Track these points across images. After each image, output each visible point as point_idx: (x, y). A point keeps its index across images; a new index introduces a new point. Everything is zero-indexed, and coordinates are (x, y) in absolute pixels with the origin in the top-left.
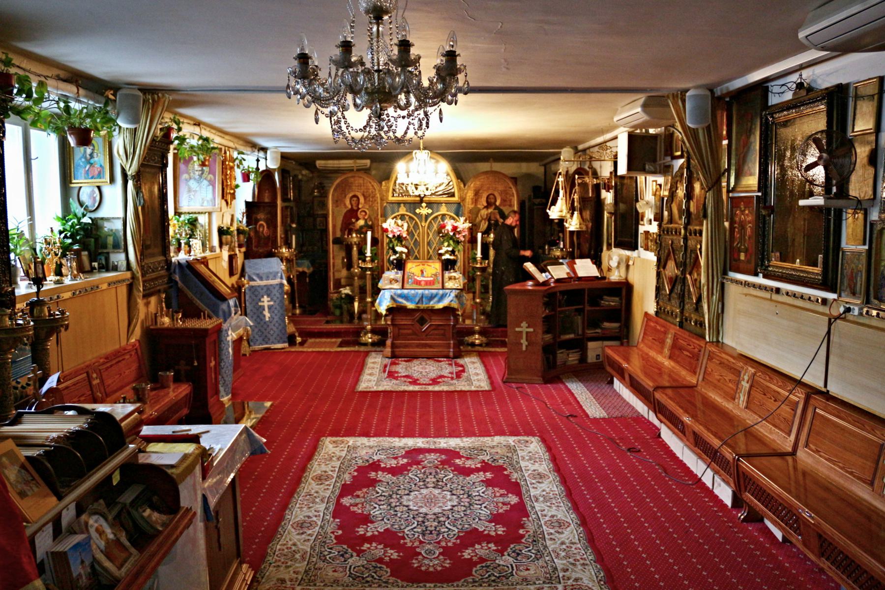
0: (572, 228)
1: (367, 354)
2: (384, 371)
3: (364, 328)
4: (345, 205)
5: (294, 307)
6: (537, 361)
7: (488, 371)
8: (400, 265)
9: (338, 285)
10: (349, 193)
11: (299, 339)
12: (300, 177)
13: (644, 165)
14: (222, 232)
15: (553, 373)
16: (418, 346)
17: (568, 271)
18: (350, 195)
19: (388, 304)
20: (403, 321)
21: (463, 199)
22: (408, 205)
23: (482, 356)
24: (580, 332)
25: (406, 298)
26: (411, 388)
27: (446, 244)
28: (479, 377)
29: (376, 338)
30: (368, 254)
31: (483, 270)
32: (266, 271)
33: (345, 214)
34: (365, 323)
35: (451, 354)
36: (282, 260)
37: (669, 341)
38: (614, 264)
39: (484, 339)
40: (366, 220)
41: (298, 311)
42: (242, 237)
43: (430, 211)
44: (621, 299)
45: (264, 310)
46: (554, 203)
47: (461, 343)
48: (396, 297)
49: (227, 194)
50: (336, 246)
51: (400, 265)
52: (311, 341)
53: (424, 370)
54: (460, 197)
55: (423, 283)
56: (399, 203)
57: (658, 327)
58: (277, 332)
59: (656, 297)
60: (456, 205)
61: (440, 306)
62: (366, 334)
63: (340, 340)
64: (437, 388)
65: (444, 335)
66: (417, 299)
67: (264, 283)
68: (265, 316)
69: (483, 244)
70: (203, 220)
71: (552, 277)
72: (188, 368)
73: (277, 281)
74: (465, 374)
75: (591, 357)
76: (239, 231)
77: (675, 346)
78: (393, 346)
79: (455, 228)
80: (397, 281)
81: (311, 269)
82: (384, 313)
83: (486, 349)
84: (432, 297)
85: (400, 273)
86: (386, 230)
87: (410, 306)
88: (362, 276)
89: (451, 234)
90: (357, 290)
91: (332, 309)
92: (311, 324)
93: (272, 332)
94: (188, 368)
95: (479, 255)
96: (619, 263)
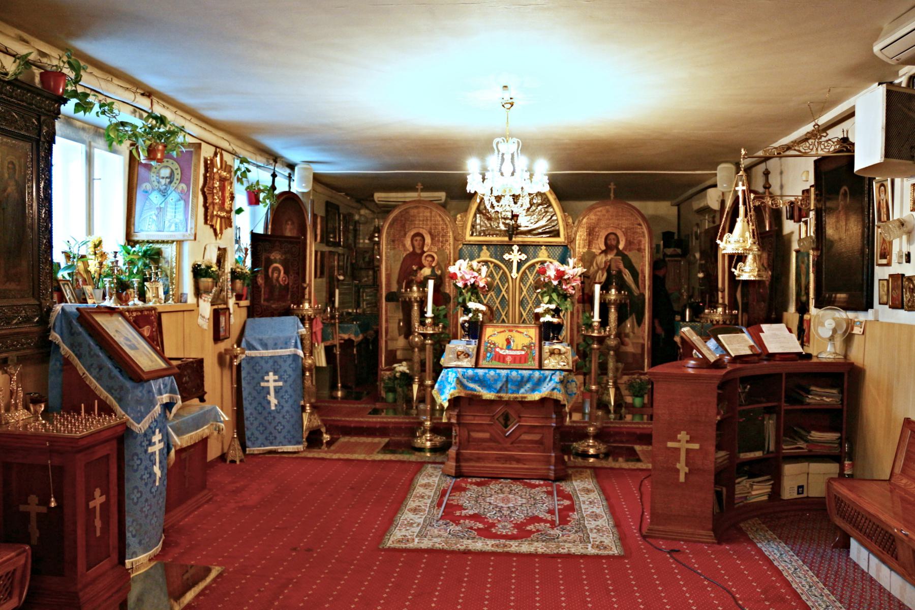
0: (745, 277)
2: (439, 505)
3: (421, 424)
4: (404, 246)
5: (334, 387)
6: (704, 500)
7: (613, 510)
8: (474, 330)
9: (393, 359)
10: (410, 230)
11: (326, 437)
12: (357, 217)
14: (198, 272)
15: (730, 523)
16: (498, 459)
17: (752, 343)
18: (412, 233)
19: (452, 391)
21: (571, 240)
22: (492, 248)
23: (598, 473)
24: (772, 448)
25: (482, 382)
26: (480, 545)
27: (546, 299)
28: (600, 522)
29: (439, 439)
30: (429, 314)
31: (601, 340)
35: (552, 474)
36: (303, 320)
39: (603, 448)
40: (433, 268)
41: (339, 394)
42: (239, 283)
43: (524, 257)
44: (842, 392)
45: (269, 393)
47: (567, 450)
48: (465, 381)
49: (217, 215)
51: (474, 330)
52: (344, 439)
53: (506, 502)
55: (509, 359)
56: (480, 245)
58: (288, 427)
60: (560, 249)
61: (536, 396)
62: (424, 433)
63: (386, 440)
64: (525, 547)
65: (540, 442)
66: (499, 385)
68: (269, 402)
70: (169, 251)
71: (728, 354)
72: (43, 509)
74: (575, 516)
75: (789, 492)
76: (235, 275)
78: (458, 458)
79: (560, 275)
80: (467, 355)
81: (361, 337)
82: (446, 405)
83: (604, 464)
84: (521, 383)
85: (474, 344)
86: (454, 276)
87: (488, 395)
88: (422, 348)
89: (555, 283)
90: (417, 367)
91: (383, 394)
92: (348, 415)
93: (279, 428)
94: (43, 509)
95: (597, 318)
96: (835, 331)
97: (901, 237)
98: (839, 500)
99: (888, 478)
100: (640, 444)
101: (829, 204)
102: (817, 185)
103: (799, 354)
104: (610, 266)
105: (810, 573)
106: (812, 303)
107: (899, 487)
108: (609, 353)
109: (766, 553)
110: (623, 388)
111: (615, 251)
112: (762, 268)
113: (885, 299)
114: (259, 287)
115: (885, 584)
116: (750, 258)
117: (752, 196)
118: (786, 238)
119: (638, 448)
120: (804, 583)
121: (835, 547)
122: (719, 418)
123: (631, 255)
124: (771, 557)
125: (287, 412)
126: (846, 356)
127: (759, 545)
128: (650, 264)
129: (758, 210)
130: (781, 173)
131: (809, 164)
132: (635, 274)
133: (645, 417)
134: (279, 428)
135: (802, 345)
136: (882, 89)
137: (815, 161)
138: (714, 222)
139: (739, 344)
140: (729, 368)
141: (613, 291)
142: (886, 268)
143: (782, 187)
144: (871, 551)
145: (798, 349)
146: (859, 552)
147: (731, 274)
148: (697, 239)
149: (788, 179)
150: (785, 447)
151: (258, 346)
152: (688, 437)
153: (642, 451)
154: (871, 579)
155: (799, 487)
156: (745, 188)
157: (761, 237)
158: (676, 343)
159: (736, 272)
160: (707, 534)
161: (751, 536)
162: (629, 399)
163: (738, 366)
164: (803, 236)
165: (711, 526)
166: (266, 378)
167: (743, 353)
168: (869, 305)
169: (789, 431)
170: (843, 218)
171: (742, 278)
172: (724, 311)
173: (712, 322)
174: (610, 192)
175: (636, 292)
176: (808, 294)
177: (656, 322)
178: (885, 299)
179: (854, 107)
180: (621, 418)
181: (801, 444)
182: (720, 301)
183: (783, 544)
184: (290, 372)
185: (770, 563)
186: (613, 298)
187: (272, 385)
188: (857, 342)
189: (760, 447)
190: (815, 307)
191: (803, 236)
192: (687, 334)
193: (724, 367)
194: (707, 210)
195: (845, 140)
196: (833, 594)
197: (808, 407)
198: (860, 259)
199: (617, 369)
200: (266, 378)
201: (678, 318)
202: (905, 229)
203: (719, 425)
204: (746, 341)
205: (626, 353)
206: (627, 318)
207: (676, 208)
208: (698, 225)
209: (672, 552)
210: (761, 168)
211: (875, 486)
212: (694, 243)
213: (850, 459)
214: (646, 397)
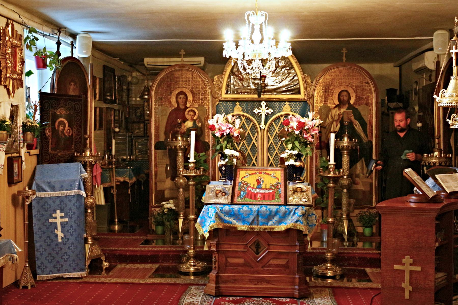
1: (185, 287)
4: (170, 103)
5: (112, 222)
8: (230, 173)
9: (161, 198)
10: (175, 89)
11: (106, 264)
16: (251, 281)
19: (212, 224)
20: (231, 247)
21: (310, 97)
22: (244, 104)
25: (236, 216)
27: (290, 146)
29: (201, 265)
31: (336, 180)
32: (61, 179)
33: (170, 113)
34: (188, 247)
35: (296, 293)
39: (339, 271)
40: (194, 121)
43: (270, 111)
45: (56, 228)
48: (222, 215)
50: (160, 152)
51: (230, 173)
52: (120, 266)
54: (307, 94)
55: (259, 197)
56: (234, 102)
61: (282, 227)
65: (286, 266)
66: (251, 218)
67: (57, 194)
68: (57, 236)
69: (336, 150)
71: (444, 191)
73: (75, 191)
78: (218, 280)
79: (301, 126)
81: (134, 179)
82: (207, 235)
84: (270, 216)
87: (242, 227)
88: (186, 188)
89: (297, 132)
90: (182, 204)
91: (154, 227)
95: (332, 162)
100: (371, 267)
108: (342, 191)
110: (354, 219)
111: (347, 106)
114: (46, 138)
119: (368, 270)
122: (437, 244)
123: (360, 108)
125: (72, 243)
132: (364, 125)
133: (374, 244)
134: (65, 257)
138: (430, 80)
140: (445, 203)
141: (346, 139)
147: (446, 124)
148: (416, 94)
151: (47, 188)
152: (411, 261)
153: (372, 273)
159: (450, 122)
162: (360, 230)
163: (453, 200)
166: (54, 215)
174: (343, 56)
175: (365, 140)
184: (74, 209)
186: (345, 144)
187: (59, 221)
192: (409, 174)
193: (442, 202)
194: (425, 69)
199: (349, 204)
200: (54, 215)
203: (438, 251)
205: (357, 191)
206: (357, 162)
207: (398, 68)
208: (416, 82)
212: (413, 98)
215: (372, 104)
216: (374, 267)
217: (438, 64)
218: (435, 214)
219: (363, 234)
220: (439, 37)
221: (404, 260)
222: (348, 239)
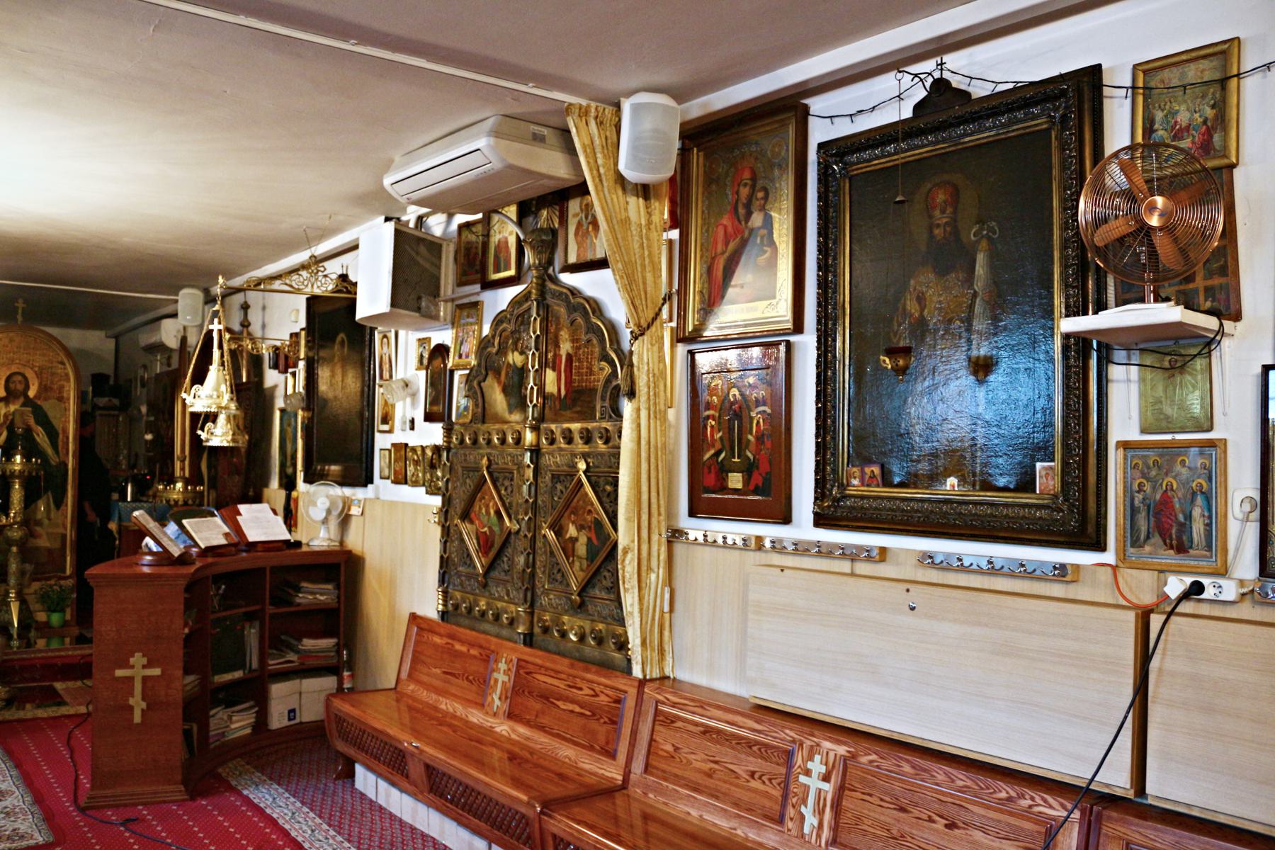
0: (215, 442)
7: (29, 780)
13: (419, 298)
17: (227, 530)
24: (255, 665)
37: (501, 676)
38: (318, 513)
44: (338, 587)
46: (199, 378)
57: (458, 647)
59: (442, 580)
71: (196, 545)
75: (278, 720)
77: (521, 688)
96: (329, 512)
97: (404, 399)
98: (340, 720)
99: (393, 685)
100: (64, 679)
101: (322, 353)
102: (309, 328)
103: (287, 542)
104: (12, 421)
105: (312, 815)
106: (300, 476)
107: (406, 694)
108: (9, 550)
109: (256, 801)
110: (31, 599)
111: (22, 400)
112: (237, 430)
113: (386, 473)
115: (395, 810)
116: (222, 419)
117: (227, 336)
118: (267, 393)
119: (59, 686)
120: (305, 828)
121: (337, 778)
122: (187, 631)
123: (46, 406)
124: (262, 805)
126: (342, 543)
127: (245, 792)
128: (76, 421)
129: (233, 353)
130: (264, 308)
131: (301, 303)
132: (52, 434)
133: (67, 640)
135: (290, 531)
136: (391, 226)
137: (308, 299)
138: (169, 365)
139: (209, 531)
140: (198, 564)
141: (18, 458)
142: (387, 435)
143: (264, 326)
144: (379, 775)
145: (285, 536)
146: (365, 778)
147: (196, 440)
148: (143, 386)
149: (273, 317)
150: (271, 662)
152: (145, 661)
153: (66, 689)
154: (381, 807)
155: (290, 711)
156: (221, 327)
157: (239, 390)
158: (111, 531)
159: (203, 435)
160: (175, 791)
161: (234, 783)
162: (41, 617)
163: (210, 560)
164: (290, 391)
165: (179, 778)
167: (215, 543)
168: (368, 480)
169: (275, 642)
170: (339, 371)
171: (211, 444)
172: (185, 488)
173: (168, 501)
174: (16, 313)
175: (54, 460)
176: (294, 465)
177: (87, 505)
178: (386, 473)
179: (357, 239)
180: (29, 645)
181: (292, 657)
182: (178, 473)
183: (276, 786)
185: (259, 811)
186: (17, 468)
188: (354, 525)
189: (242, 666)
190: (305, 481)
191: (290, 391)
192: (141, 520)
193: (193, 563)
194: (160, 347)
195: (344, 277)
196: (339, 833)
197: (300, 608)
198: (358, 423)
199: (22, 573)
201: (115, 496)
202: (409, 390)
203: (188, 640)
204: (219, 527)
205: (37, 549)
206: (39, 497)
207: (113, 341)
208: (145, 367)
209: (126, 822)
210: (238, 299)
211: (380, 698)
212: (139, 391)
213: (350, 669)
214: (68, 611)
215: (69, 399)
216: (70, 680)
217: (184, 340)
218: (183, 583)
219: (47, 624)
220: (188, 299)
221: (132, 660)
222: (19, 635)
